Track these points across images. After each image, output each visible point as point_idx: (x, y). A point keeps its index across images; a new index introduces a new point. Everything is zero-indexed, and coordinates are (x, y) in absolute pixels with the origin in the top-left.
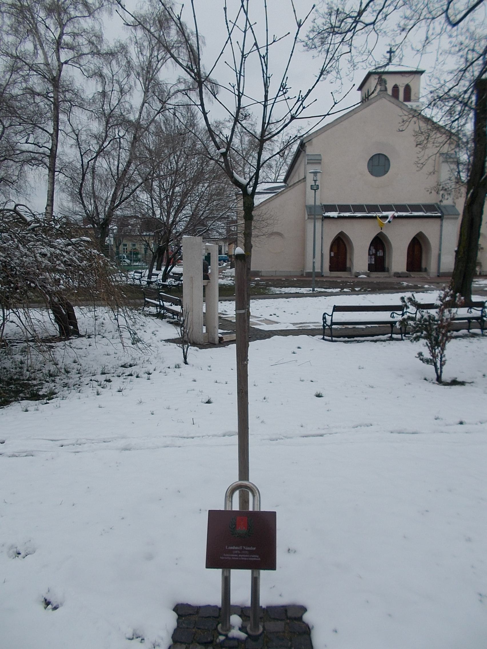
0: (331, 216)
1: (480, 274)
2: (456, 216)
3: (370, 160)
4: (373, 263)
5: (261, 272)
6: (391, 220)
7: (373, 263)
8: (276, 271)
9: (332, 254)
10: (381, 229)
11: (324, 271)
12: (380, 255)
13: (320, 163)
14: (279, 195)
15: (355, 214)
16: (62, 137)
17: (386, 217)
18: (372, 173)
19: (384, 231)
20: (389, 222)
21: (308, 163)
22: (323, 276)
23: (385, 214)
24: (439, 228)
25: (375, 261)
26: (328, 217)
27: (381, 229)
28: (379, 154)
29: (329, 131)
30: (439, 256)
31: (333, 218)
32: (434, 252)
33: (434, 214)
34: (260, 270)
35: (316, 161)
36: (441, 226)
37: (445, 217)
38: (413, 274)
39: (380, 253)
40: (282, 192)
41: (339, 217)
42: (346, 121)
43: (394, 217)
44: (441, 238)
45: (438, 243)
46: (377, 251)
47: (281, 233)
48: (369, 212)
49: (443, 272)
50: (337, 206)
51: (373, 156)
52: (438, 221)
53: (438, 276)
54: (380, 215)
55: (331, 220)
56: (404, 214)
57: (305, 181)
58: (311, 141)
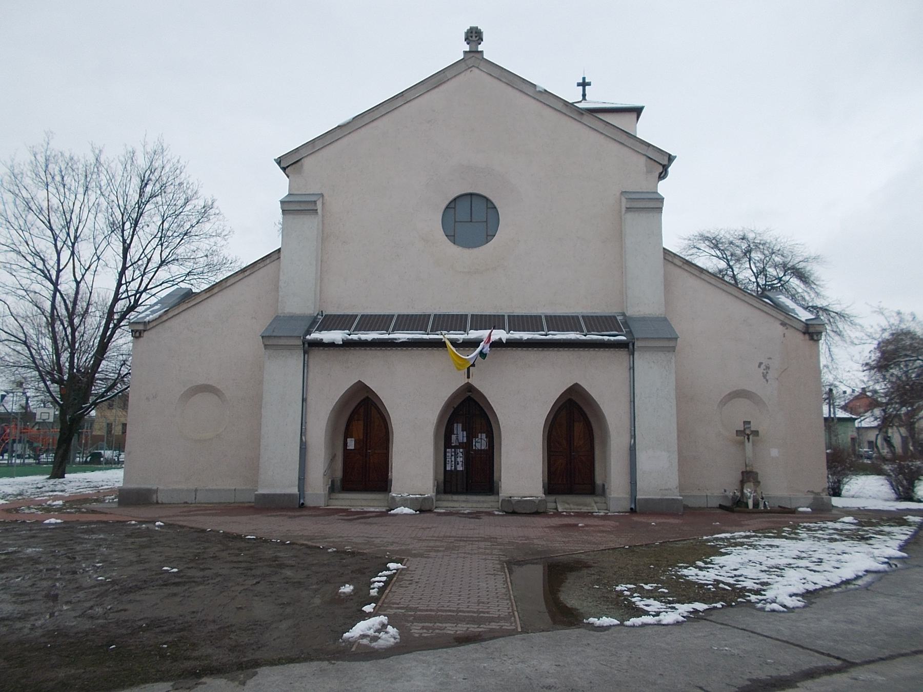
0: (325, 341)
1: (756, 505)
2: (671, 344)
3: (447, 207)
4: (460, 468)
5: (156, 491)
6: (487, 349)
7: (460, 468)
8: (196, 490)
9: (351, 444)
10: (468, 377)
11: (309, 491)
12: (478, 446)
13: (673, 349)
14: (216, 290)
15: (392, 336)
16: (47, 234)
17: (475, 344)
18: (452, 237)
19: (475, 382)
20: (482, 355)
21: (628, 209)
22: (302, 506)
23: (473, 334)
24: (626, 374)
25: (468, 462)
26: (319, 344)
27: (468, 377)
28: (471, 195)
29: (344, 141)
30: (632, 450)
31: (332, 345)
32: (617, 442)
33: (606, 338)
34: (155, 488)
35: (303, 207)
36: (632, 368)
37: (637, 344)
38: (565, 504)
39: (480, 443)
40: (224, 285)
41: (348, 344)
42: (385, 119)
43: (497, 345)
44: (633, 402)
45: (625, 407)
46: (471, 436)
47: (218, 390)
48: (433, 330)
49: (647, 500)
50: (581, 319)
51: (455, 199)
52: (622, 354)
53: (632, 511)
54: (460, 336)
55: (332, 352)
56: (525, 336)
57: (279, 258)
58: (299, 163)
